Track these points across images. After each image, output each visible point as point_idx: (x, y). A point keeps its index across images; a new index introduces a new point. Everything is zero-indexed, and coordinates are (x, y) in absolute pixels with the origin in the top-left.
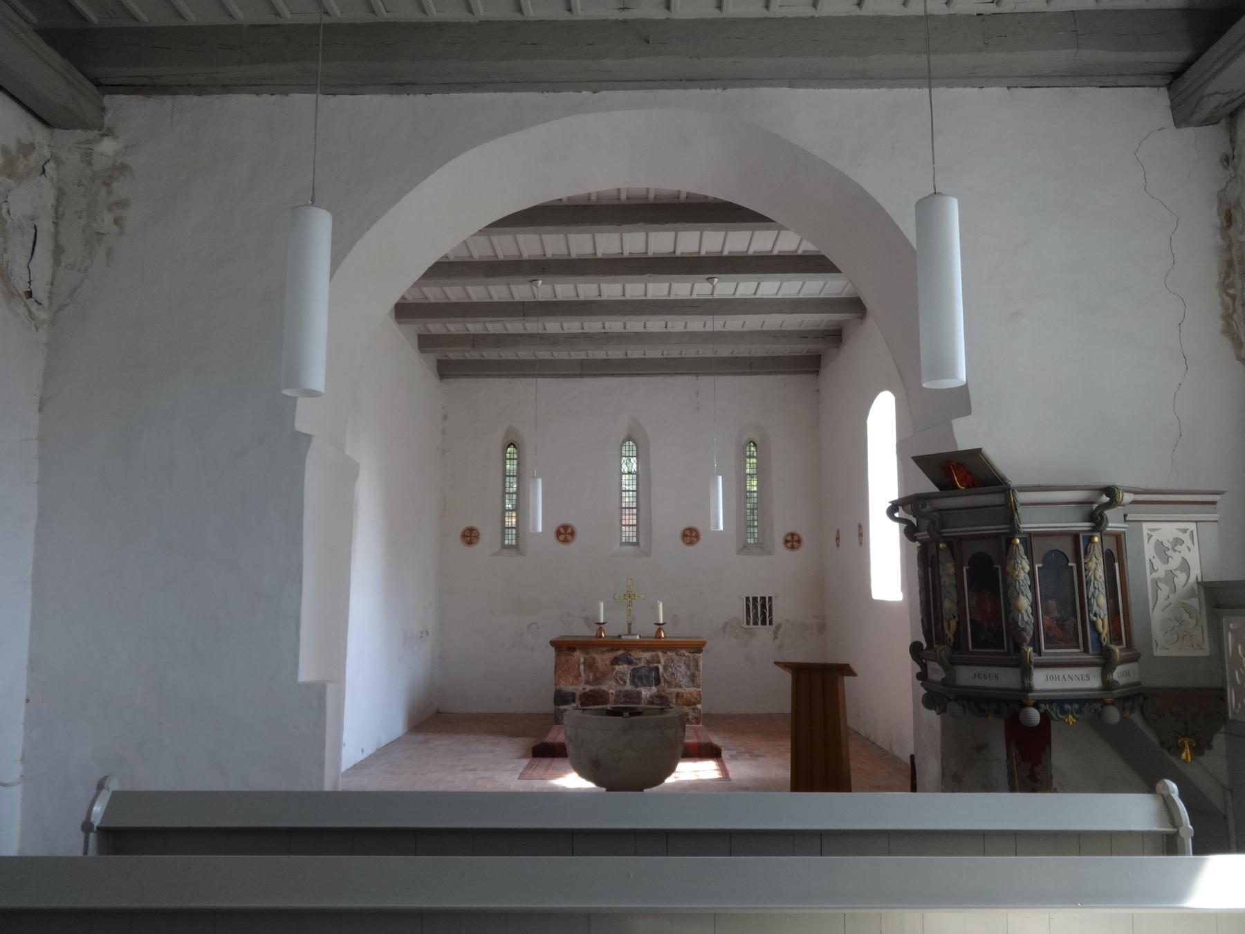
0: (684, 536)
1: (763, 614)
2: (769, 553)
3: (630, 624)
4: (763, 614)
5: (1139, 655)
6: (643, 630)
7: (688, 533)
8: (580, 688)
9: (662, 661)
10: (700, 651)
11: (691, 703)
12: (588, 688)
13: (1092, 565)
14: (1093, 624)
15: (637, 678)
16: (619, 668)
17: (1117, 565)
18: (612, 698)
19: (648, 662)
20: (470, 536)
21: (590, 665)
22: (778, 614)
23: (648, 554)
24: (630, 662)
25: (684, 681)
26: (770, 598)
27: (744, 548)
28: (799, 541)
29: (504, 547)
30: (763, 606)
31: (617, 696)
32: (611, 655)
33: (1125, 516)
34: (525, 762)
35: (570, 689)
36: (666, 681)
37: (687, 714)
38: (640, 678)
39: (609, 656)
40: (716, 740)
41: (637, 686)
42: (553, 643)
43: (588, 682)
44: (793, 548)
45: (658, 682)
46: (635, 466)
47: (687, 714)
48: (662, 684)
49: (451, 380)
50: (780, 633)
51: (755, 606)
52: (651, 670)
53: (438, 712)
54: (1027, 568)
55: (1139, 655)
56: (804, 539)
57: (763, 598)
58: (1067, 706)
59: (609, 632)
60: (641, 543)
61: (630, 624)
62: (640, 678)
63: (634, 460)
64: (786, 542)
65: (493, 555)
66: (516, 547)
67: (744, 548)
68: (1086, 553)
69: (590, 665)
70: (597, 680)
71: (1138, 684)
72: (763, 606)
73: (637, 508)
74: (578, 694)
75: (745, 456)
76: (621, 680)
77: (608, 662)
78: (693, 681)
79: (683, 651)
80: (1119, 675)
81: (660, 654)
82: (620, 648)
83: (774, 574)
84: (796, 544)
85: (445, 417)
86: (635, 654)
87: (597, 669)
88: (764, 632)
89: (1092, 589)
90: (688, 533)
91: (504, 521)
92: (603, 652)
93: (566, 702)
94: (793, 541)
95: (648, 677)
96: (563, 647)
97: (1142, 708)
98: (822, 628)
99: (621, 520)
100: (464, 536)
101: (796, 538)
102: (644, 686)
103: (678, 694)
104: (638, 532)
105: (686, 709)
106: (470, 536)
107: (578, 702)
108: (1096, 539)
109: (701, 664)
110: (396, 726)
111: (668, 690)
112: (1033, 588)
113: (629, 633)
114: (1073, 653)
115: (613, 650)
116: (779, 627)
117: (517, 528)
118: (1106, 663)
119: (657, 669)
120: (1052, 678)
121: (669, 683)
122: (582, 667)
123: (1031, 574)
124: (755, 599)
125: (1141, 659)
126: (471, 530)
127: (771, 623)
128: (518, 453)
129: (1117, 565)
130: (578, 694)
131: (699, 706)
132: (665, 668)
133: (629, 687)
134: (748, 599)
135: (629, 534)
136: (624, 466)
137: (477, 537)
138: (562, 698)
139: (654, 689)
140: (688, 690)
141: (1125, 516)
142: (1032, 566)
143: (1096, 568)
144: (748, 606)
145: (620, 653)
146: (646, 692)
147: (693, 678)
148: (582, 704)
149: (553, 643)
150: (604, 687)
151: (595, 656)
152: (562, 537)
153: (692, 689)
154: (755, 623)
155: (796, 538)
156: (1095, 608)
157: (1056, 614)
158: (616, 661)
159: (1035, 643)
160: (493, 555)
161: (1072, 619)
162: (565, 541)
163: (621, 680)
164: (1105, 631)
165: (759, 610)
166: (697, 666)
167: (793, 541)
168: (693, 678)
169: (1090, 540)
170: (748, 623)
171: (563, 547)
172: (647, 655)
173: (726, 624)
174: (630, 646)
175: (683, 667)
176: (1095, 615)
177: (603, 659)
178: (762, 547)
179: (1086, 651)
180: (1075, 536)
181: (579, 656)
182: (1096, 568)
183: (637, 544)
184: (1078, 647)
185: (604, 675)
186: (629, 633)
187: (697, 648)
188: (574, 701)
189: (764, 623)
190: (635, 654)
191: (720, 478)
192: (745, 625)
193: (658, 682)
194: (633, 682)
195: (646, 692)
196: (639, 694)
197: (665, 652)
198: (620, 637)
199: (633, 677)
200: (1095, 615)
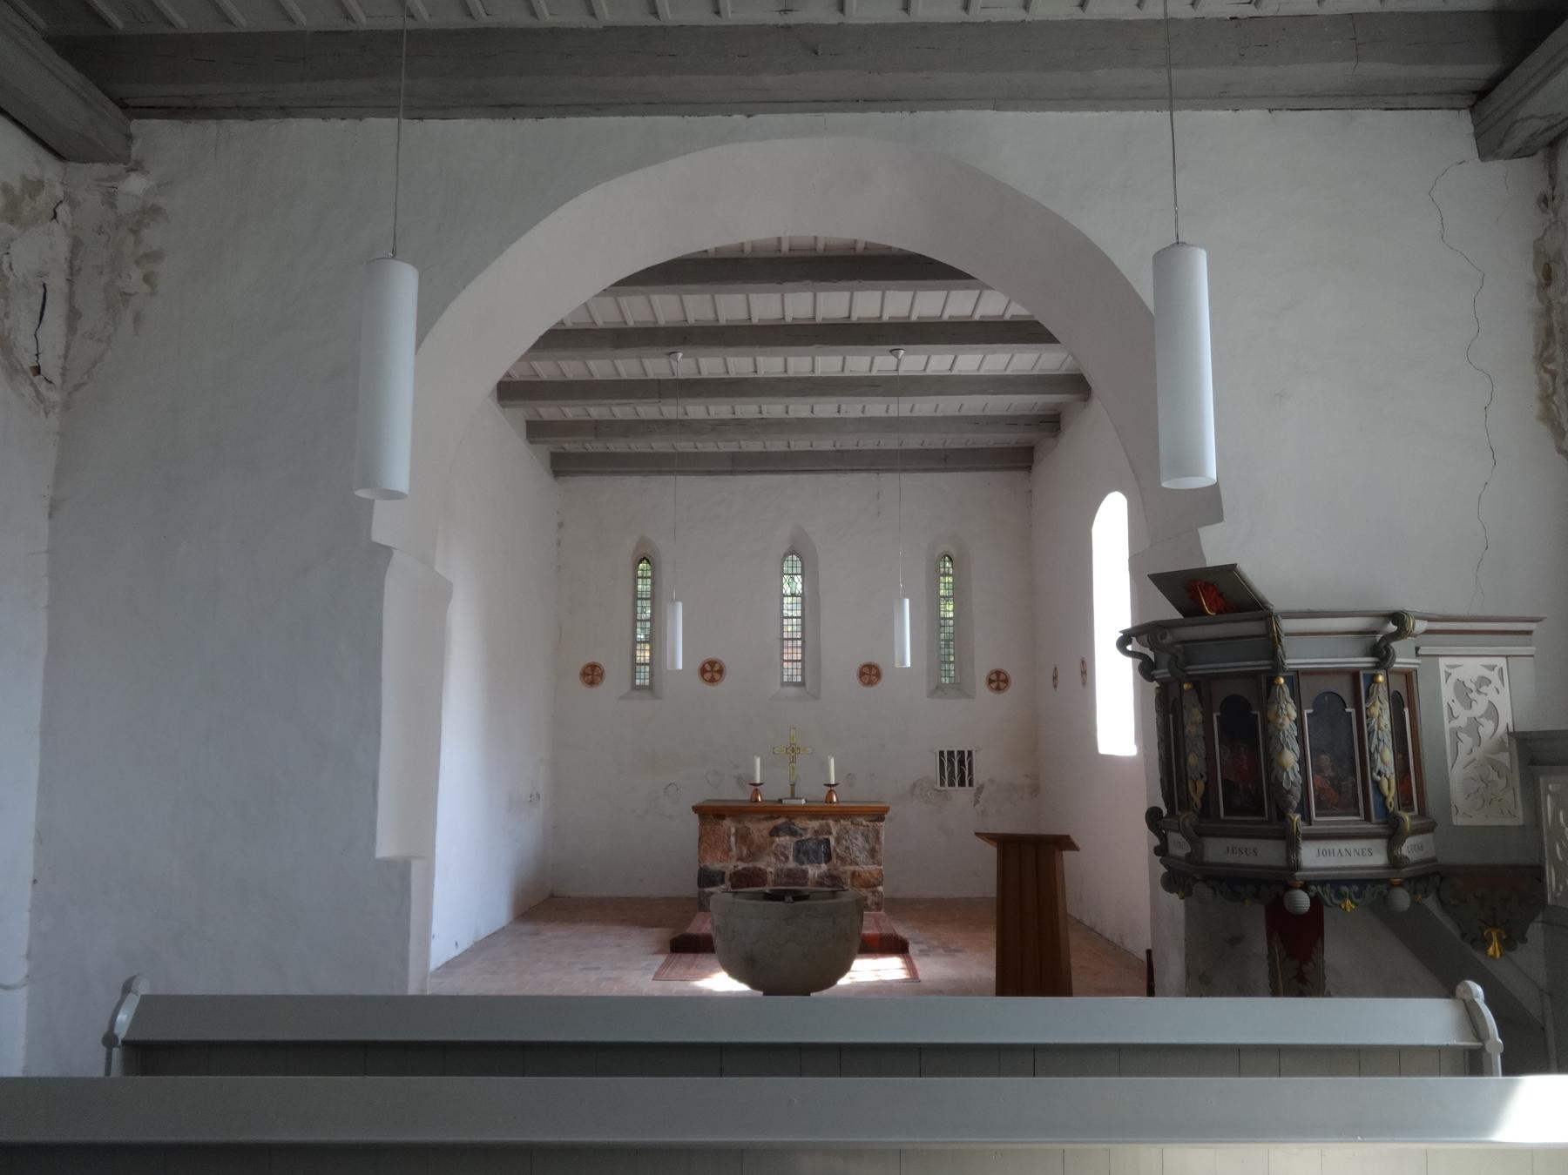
0: (862, 674)
1: (962, 772)
2: (969, 696)
3: (793, 785)
4: (962, 772)
5: (1435, 824)
6: (810, 792)
7: (866, 670)
8: (731, 866)
9: (834, 831)
10: (882, 819)
11: (871, 885)
12: (741, 865)
13: (1375, 711)
14: (1377, 785)
15: (802, 853)
16: (779, 840)
17: (1406, 710)
18: (771, 878)
19: (816, 833)
20: (592, 674)
21: (743, 837)
22: (980, 773)
23: (816, 697)
24: (793, 833)
25: (862, 857)
26: (970, 753)
27: (938, 690)
28: (1006, 681)
29: (635, 688)
30: (961, 762)
31: (777, 875)
32: (770, 825)
33: (1417, 649)
34: (662, 958)
35: (718, 866)
36: (839, 857)
37: (865, 898)
38: (806, 853)
39: (767, 825)
40: (902, 931)
41: (802, 863)
42: (696, 809)
43: (740, 859)
44: (998, 689)
45: (828, 858)
46: (799, 586)
47: (865, 898)
48: (834, 860)
49: (568, 478)
50: (983, 796)
51: (951, 763)
52: (819, 843)
53: (552, 896)
54: (1294, 715)
55: (1435, 824)
56: (1013, 678)
57: (961, 753)
58: (1344, 889)
59: (767, 795)
60: (808, 683)
61: (793, 785)
62: (806, 853)
63: (798, 579)
64: (990, 681)
65: (622, 698)
66: (650, 688)
67: (938, 690)
68: (1368, 695)
69: (743, 837)
70: (752, 856)
71: (1434, 860)
72: (961, 762)
73: (802, 639)
74: (728, 873)
75: (938, 574)
76: (782, 855)
77: (765, 833)
78: (873, 857)
79: (860, 819)
80: (1409, 849)
81: (831, 822)
82: (781, 816)
83: (974, 722)
84: (1002, 685)
85: (561, 525)
86: (800, 823)
87: (752, 842)
88: (962, 796)
89: (1375, 741)
90: (866, 670)
91: (634, 656)
92: (759, 820)
93: (713, 884)
94: (998, 681)
95: (816, 852)
96: (710, 814)
97: (1438, 890)
98: (1035, 790)
99: (782, 654)
100: (584, 674)
101: (1002, 677)
102: (811, 862)
103: (854, 873)
104: (803, 669)
105: (864, 892)
106: (592, 674)
107: (728, 883)
108: (1381, 678)
109: (883, 836)
110: (499, 914)
111: (842, 868)
112: (1300, 739)
113: (793, 796)
114: (1351, 821)
115: (772, 818)
116: (981, 789)
117: (651, 664)
118: (1393, 834)
119: (828, 841)
120: (1325, 853)
121: (843, 860)
122: (733, 839)
123: (1299, 722)
124: (951, 753)
125: (1437, 829)
126: (593, 666)
127: (971, 784)
128: (653, 570)
129: (1406, 710)
130: (728, 873)
131: (880, 888)
132: (838, 840)
133: (792, 864)
134: (941, 753)
135: (792, 671)
136: (786, 586)
137: (601, 675)
138: (707, 878)
139: (824, 867)
140: (867, 868)
141: (1417, 649)
142: (1300, 712)
143: (1381, 714)
144: (942, 762)
145: (781, 821)
146: (814, 871)
147: (873, 853)
148: (733, 886)
149: (696, 809)
150: (761, 865)
151: (750, 825)
152: (708, 676)
153: (872, 867)
154: (951, 784)
155: (1002, 677)
156: (1379, 765)
157: (1330, 773)
158: (775, 832)
159: (1304, 809)
160: (622, 698)
161: (1351, 778)
162: (712, 681)
163: (782, 855)
164: (1391, 794)
165: (956, 768)
166: (878, 838)
167: (998, 681)
168: (873, 853)
169: (1372, 679)
170: (942, 784)
171: (709, 688)
172: (815, 824)
173: (914, 785)
174: (794, 813)
175: (860, 839)
176: (1380, 774)
177: (759, 829)
178: (959, 688)
179: (1368, 819)
180: (1354, 675)
181: (729, 825)
182: (1381, 714)
183: (802, 684)
184: (1358, 814)
185: (761, 849)
186: (793, 796)
187: (878, 815)
188: (723, 882)
189: (962, 784)
190: (800, 823)
191: (907, 601)
192: (938, 786)
193: (828, 858)
194: (797, 859)
195: (814, 871)
196: (805, 873)
197: (837, 821)
198: (780, 801)
199: (798, 851)
200: (1380, 774)
